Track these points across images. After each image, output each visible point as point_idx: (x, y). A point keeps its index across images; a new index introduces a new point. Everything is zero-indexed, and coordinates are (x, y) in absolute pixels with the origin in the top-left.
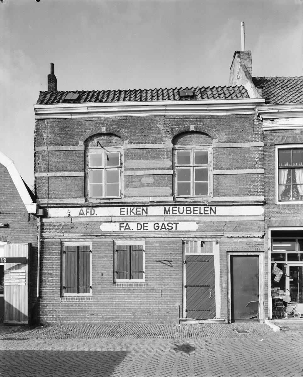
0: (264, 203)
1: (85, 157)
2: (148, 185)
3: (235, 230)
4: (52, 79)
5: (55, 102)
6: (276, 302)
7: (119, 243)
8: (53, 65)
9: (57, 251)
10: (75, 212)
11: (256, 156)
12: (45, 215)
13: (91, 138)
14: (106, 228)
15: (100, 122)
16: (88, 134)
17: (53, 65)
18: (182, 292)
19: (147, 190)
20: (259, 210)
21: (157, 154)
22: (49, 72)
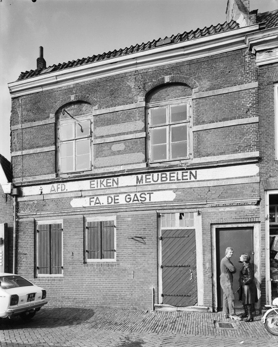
0: (259, 160)
2: (119, 152)
7: (90, 219)
9: (31, 230)
10: (46, 189)
12: (20, 194)
14: (76, 203)
16: (58, 105)
19: (118, 159)
20: (253, 169)
21: (128, 116)
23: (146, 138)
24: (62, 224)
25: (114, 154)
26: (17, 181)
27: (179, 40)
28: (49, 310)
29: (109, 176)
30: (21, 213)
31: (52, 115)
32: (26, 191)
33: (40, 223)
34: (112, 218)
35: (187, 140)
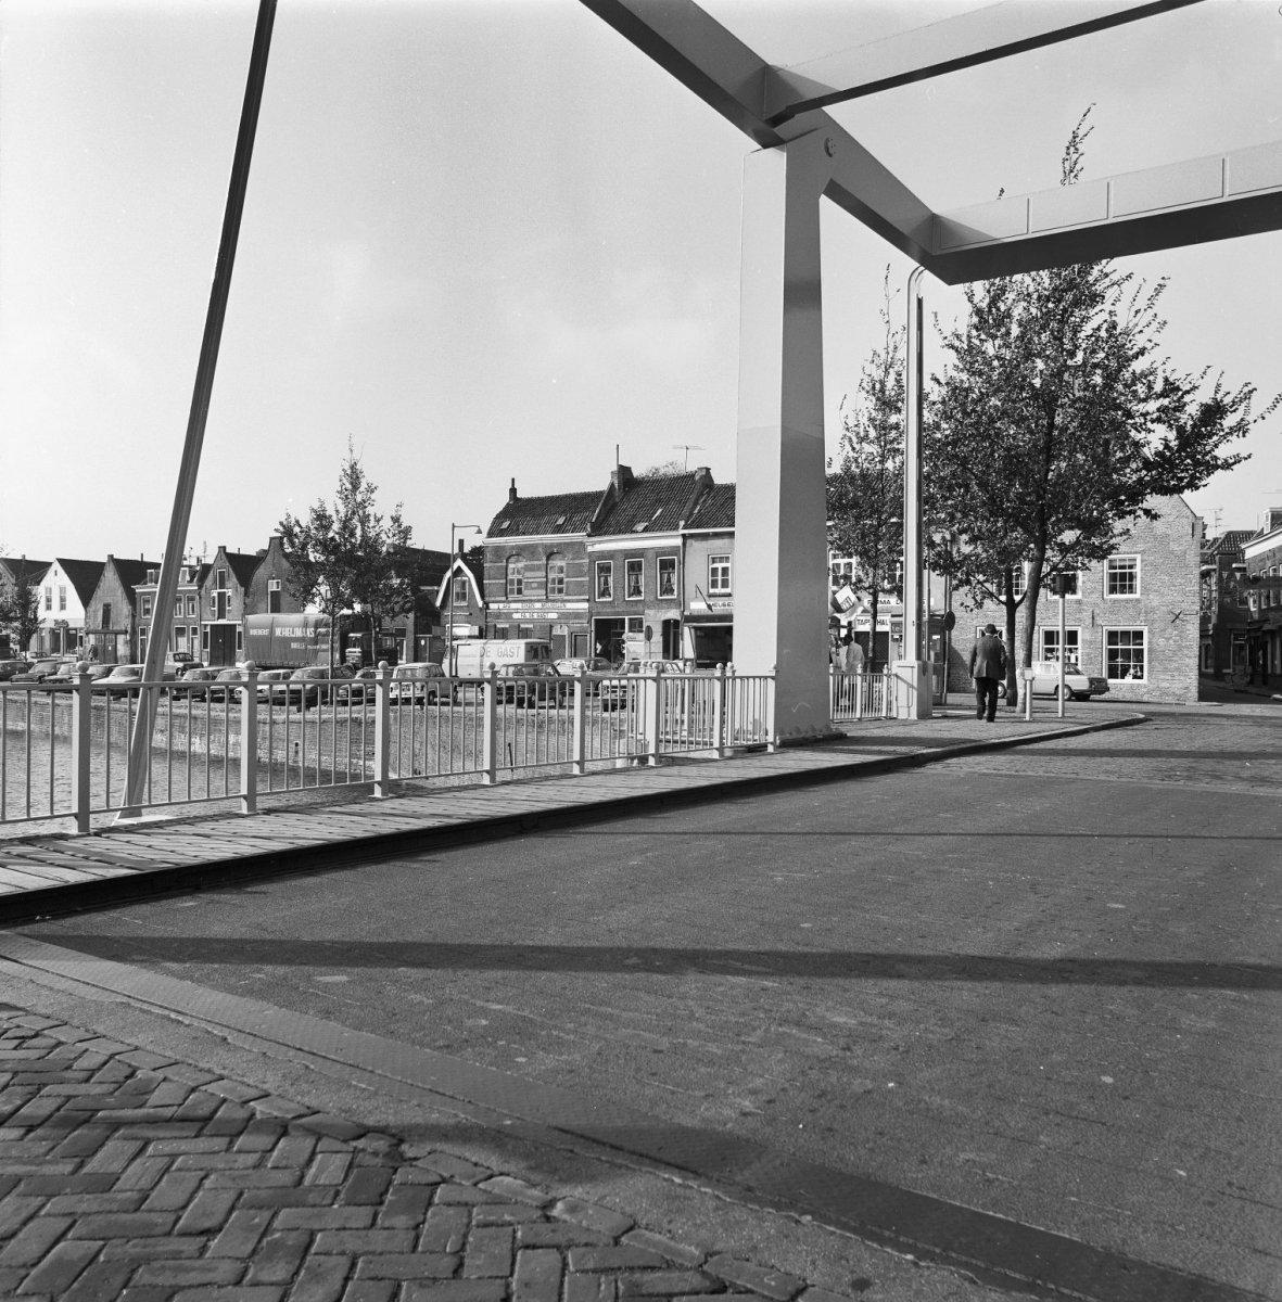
0: (588, 601)
1: (507, 569)
2: (535, 588)
3: (575, 618)
4: (513, 491)
5: (117, 1135)
6: (1214, 567)
7: (522, 626)
8: (513, 480)
9: (493, 630)
10: (501, 606)
11: (586, 569)
12: (488, 608)
13: (509, 557)
14: (515, 616)
15: (513, 547)
16: (508, 554)
17: (513, 480)
18: (7, 800)
19: (534, 592)
20: (586, 605)
21: (538, 568)
22: (510, 486)
23: (547, 582)
24: (529, 640)
25: (533, 589)
26: (487, 599)
27: (14, 677)
28: (1003, 1290)
29: (1040, 737)
30: (489, 620)
31: (544, 558)
32: (492, 606)
33: (498, 626)
34: (531, 626)
35: (1076, 644)
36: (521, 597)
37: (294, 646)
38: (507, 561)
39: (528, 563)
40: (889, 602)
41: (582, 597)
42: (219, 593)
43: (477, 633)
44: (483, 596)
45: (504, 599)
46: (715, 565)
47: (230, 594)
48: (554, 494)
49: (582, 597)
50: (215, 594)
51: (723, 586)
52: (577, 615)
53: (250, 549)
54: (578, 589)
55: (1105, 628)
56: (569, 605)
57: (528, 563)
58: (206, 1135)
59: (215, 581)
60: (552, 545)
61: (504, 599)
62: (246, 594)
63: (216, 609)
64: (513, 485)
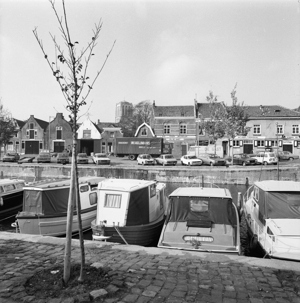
0: (196, 135)
3: (190, 140)
8: (154, 101)
11: (195, 127)
13: (165, 123)
15: (166, 120)
16: (164, 122)
20: (195, 137)
22: (153, 103)
31: (179, 124)
36: (169, 134)
37: (140, 147)
38: (164, 124)
39: (172, 124)
40: (293, 138)
41: (193, 134)
42: (30, 130)
43: (231, 145)
44: (154, 133)
45: (163, 134)
46: (278, 127)
47: (36, 131)
48: (20, 120)
49: (193, 134)
50: (28, 130)
51: (258, 133)
52: (191, 139)
53: (23, 119)
54: (192, 132)
55: (15, 141)
56: (188, 137)
57: (172, 124)
58: (105, 290)
59: (28, 126)
60: (182, 120)
61: (163, 134)
62: (45, 131)
63: (29, 135)
64: (154, 102)
